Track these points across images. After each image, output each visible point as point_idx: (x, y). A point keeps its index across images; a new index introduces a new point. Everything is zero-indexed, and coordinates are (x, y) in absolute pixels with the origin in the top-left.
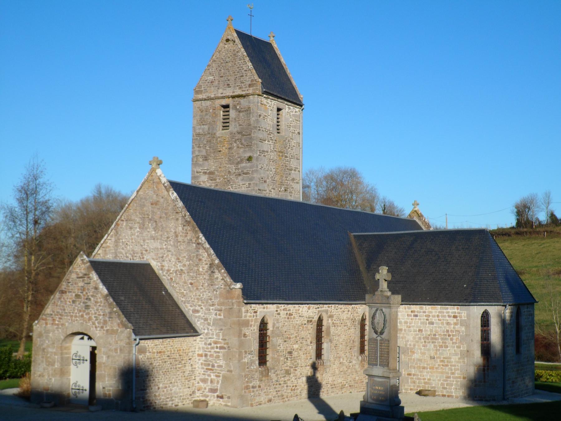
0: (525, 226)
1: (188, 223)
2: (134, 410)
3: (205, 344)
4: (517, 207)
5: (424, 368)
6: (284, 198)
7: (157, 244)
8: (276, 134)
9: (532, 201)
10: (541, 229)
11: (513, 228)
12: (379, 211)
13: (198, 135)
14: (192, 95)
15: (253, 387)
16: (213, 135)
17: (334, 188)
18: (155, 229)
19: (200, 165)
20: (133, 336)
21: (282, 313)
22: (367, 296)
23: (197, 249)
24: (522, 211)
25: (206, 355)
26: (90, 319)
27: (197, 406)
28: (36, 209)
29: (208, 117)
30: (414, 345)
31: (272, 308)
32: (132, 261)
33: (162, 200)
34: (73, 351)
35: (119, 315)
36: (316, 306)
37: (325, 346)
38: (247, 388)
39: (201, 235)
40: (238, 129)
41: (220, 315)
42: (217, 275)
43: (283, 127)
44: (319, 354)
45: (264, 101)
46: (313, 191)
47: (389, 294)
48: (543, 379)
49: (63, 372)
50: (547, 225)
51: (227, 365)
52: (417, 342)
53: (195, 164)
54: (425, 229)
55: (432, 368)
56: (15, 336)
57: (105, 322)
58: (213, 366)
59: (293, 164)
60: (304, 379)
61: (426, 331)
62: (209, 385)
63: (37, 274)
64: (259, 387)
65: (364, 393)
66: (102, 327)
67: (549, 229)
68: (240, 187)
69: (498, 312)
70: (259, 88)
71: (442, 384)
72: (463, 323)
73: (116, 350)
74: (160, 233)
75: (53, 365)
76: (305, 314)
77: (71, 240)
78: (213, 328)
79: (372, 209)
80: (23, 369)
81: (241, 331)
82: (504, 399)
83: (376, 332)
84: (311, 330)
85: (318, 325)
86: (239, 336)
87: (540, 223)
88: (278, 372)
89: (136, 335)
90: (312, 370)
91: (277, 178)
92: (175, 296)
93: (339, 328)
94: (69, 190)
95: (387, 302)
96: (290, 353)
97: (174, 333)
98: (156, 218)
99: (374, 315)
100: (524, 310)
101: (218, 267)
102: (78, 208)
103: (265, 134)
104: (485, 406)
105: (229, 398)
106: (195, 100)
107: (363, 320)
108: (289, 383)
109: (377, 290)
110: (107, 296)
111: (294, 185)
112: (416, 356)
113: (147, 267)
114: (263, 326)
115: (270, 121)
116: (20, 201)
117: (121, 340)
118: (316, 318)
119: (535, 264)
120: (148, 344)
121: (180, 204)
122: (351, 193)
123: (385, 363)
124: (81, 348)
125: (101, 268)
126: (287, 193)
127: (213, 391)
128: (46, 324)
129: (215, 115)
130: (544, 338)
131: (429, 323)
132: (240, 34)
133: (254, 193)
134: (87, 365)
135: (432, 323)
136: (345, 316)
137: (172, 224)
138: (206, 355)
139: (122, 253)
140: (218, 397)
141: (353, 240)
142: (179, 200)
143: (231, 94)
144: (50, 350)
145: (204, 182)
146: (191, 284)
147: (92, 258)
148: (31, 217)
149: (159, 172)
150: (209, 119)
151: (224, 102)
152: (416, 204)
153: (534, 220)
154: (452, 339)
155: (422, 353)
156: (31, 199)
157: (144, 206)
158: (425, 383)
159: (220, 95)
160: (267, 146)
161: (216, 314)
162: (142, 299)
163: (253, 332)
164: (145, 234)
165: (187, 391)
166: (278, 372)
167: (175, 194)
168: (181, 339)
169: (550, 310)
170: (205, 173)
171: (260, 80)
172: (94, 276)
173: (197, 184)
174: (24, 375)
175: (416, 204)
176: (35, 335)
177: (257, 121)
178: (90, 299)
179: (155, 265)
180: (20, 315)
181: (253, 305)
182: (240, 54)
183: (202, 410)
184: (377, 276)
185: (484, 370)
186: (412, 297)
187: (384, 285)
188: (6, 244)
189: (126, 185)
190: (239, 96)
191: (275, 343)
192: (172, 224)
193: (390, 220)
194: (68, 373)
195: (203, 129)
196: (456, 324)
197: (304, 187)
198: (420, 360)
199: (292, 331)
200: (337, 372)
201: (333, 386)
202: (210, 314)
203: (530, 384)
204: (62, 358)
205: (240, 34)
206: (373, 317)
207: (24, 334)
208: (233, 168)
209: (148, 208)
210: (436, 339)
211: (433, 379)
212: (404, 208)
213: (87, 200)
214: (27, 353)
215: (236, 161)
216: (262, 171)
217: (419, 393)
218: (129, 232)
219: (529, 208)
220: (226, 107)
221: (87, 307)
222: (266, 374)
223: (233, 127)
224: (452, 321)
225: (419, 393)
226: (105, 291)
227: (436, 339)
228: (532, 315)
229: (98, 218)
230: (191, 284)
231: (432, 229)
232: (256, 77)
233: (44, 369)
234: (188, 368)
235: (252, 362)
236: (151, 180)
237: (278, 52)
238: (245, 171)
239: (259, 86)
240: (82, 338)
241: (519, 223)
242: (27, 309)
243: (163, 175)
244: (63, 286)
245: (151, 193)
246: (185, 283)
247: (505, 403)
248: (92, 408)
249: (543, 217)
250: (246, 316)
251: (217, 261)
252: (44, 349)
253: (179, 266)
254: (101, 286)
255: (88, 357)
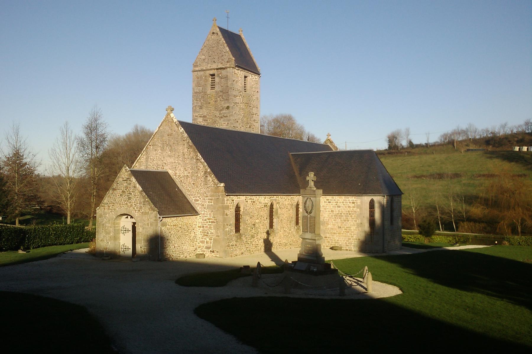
0: (394, 149)
1: (191, 146)
2: (160, 260)
3: (203, 220)
4: (389, 137)
5: (334, 233)
6: (249, 132)
7: (172, 160)
8: (244, 92)
9: (398, 134)
10: (403, 151)
11: (386, 150)
12: (305, 139)
13: (196, 93)
14: (192, 68)
15: (232, 246)
16: (205, 93)
17: (278, 126)
18: (170, 151)
19: (198, 112)
20: (159, 216)
21: (249, 201)
22: (301, 191)
23: (197, 163)
24: (392, 139)
25: (203, 227)
26: (131, 206)
27: (198, 258)
28: (97, 139)
29: (202, 81)
30: (329, 220)
31: (243, 198)
32: (157, 170)
33: (174, 133)
34: (122, 225)
35: (149, 203)
36: (269, 197)
37: (275, 220)
38: (228, 246)
39: (199, 154)
40: (220, 89)
41: (211, 202)
42: (209, 178)
43: (248, 87)
44: (271, 226)
45: (236, 71)
46: (266, 129)
47: (315, 189)
48: (406, 240)
49: (116, 238)
50: (407, 148)
51: (216, 232)
52: (330, 218)
53: (194, 111)
54: (334, 150)
55: (339, 233)
56: (87, 216)
57: (141, 208)
58: (208, 233)
59: (254, 111)
60: (262, 240)
61: (336, 211)
62: (205, 245)
63: (99, 179)
64: (236, 245)
65: (300, 249)
66: (139, 211)
67: (408, 150)
68: (222, 125)
69: (380, 199)
70: (233, 63)
71: (346, 243)
72: (358, 207)
73: (148, 224)
74: (174, 153)
75: (109, 233)
76: (263, 202)
77: (120, 159)
78: (207, 210)
79: (301, 139)
80: (91, 237)
81: (224, 212)
82: (383, 252)
83: (307, 212)
84: (267, 211)
85: (270, 208)
86: (223, 214)
87: (403, 147)
88: (247, 236)
89: (160, 215)
90: (266, 235)
91: (245, 119)
92: (184, 191)
93: (283, 210)
94: (118, 128)
95: (314, 194)
96: (254, 225)
97: (183, 214)
98: (171, 143)
99: (306, 201)
100: (396, 199)
101: (209, 174)
102: (124, 139)
103: (237, 92)
104: (372, 257)
105: (217, 252)
106: (194, 71)
107: (298, 205)
108: (254, 243)
109: (307, 187)
110: (142, 191)
111: (255, 124)
112: (329, 226)
113: (166, 174)
114: (238, 209)
115: (240, 84)
116: (87, 134)
117: (151, 218)
118: (269, 204)
119: (400, 172)
120: (168, 220)
121: (186, 135)
122: (289, 129)
123: (313, 231)
124: (127, 223)
125: (137, 174)
126: (251, 129)
127: (208, 248)
128: (104, 209)
129: (206, 80)
130: (406, 215)
131: (338, 207)
132: (221, 30)
133: (231, 129)
134: (131, 233)
135: (339, 207)
136: (286, 203)
137: (181, 148)
138: (203, 227)
139: (150, 165)
140: (211, 251)
141: (291, 157)
142: (185, 132)
143: (216, 67)
144: (107, 225)
145: (200, 122)
146: (193, 184)
147: (132, 169)
148: (94, 144)
149: (172, 115)
150: (202, 82)
151: (212, 72)
152: (329, 135)
153: (399, 145)
154: (351, 216)
155: (333, 225)
156: (93, 133)
157: (163, 136)
158: (335, 242)
159: (209, 68)
160: (238, 100)
161: (209, 202)
162: (163, 193)
163: (231, 213)
164: (164, 154)
165: (192, 248)
166: (247, 236)
167: (182, 129)
168: (187, 217)
169: (410, 199)
170: (201, 116)
171: (234, 59)
172: (134, 180)
173: (196, 123)
174: (92, 240)
175: (329, 135)
176: (97, 216)
177: (232, 84)
178: (131, 194)
179: (170, 172)
180: (89, 204)
181: (231, 197)
182: (221, 42)
183: (201, 260)
184: (308, 178)
185: (371, 235)
186: (328, 191)
187: (312, 184)
188: (79, 161)
189: (152, 125)
190: (221, 69)
191: (245, 219)
192: (181, 148)
193: (312, 145)
194: (119, 238)
195: (199, 89)
196: (354, 207)
197: (261, 126)
198: (332, 229)
199: (255, 212)
200: (282, 236)
201: (280, 244)
202: (205, 202)
203: (398, 243)
204: (115, 230)
205: (221, 30)
206: (305, 203)
207: (92, 215)
208: (217, 114)
209: (166, 138)
210: (342, 216)
211: (340, 240)
212: (322, 139)
213: (130, 135)
214: (94, 227)
215: (219, 109)
216: (235, 115)
217: (332, 248)
218: (155, 153)
219: (396, 138)
220: (213, 75)
221: (129, 198)
222: (240, 237)
223: (217, 88)
224: (352, 205)
225: (332, 248)
226: (141, 189)
227: (342, 216)
228: (401, 202)
229: (135, 145)
230: (193, 184)
231: (338, 150)
232: (231, 56)
233: (104, 237)
234: (193, 234)
235: (231, 230)
236: (167, 120)
237: (245, 41)
238: (225, 115)
239: (233, 62)
240: (127, 217)
241: (390, 147)
242: (93, 200)
243: (175, 117)
244: (115, 185)
245: (167, 128)
246: (190, 183)
247: (384, 254)
248: (134, 260)
249: (404, 143)
250: (227, 203)
251: (209, 170)
252: (103, 224)
253: (186, 173)
254: (138, 185)
255: (131, 229)
